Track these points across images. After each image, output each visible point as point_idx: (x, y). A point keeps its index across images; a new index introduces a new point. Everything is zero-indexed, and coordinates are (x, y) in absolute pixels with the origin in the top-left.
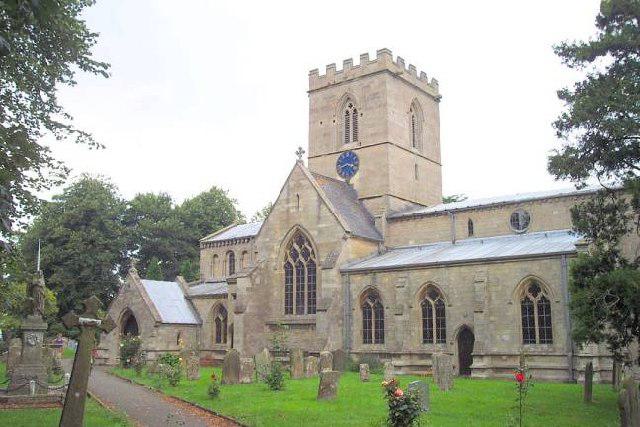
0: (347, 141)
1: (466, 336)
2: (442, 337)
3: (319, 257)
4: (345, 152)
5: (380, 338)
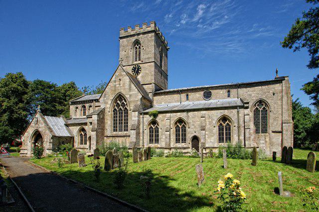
0: (136, 61)
1: (195, 139)
2: (184, 140)
3: (130, 107)
4: (135, 65)
5: (157, 141)
